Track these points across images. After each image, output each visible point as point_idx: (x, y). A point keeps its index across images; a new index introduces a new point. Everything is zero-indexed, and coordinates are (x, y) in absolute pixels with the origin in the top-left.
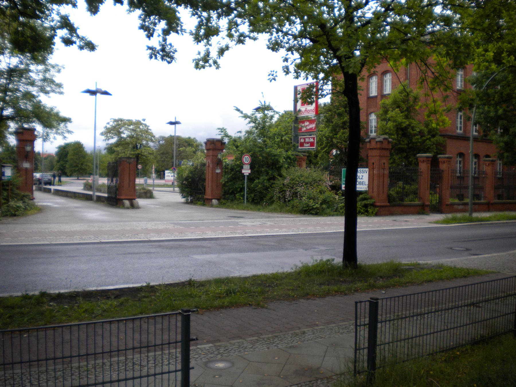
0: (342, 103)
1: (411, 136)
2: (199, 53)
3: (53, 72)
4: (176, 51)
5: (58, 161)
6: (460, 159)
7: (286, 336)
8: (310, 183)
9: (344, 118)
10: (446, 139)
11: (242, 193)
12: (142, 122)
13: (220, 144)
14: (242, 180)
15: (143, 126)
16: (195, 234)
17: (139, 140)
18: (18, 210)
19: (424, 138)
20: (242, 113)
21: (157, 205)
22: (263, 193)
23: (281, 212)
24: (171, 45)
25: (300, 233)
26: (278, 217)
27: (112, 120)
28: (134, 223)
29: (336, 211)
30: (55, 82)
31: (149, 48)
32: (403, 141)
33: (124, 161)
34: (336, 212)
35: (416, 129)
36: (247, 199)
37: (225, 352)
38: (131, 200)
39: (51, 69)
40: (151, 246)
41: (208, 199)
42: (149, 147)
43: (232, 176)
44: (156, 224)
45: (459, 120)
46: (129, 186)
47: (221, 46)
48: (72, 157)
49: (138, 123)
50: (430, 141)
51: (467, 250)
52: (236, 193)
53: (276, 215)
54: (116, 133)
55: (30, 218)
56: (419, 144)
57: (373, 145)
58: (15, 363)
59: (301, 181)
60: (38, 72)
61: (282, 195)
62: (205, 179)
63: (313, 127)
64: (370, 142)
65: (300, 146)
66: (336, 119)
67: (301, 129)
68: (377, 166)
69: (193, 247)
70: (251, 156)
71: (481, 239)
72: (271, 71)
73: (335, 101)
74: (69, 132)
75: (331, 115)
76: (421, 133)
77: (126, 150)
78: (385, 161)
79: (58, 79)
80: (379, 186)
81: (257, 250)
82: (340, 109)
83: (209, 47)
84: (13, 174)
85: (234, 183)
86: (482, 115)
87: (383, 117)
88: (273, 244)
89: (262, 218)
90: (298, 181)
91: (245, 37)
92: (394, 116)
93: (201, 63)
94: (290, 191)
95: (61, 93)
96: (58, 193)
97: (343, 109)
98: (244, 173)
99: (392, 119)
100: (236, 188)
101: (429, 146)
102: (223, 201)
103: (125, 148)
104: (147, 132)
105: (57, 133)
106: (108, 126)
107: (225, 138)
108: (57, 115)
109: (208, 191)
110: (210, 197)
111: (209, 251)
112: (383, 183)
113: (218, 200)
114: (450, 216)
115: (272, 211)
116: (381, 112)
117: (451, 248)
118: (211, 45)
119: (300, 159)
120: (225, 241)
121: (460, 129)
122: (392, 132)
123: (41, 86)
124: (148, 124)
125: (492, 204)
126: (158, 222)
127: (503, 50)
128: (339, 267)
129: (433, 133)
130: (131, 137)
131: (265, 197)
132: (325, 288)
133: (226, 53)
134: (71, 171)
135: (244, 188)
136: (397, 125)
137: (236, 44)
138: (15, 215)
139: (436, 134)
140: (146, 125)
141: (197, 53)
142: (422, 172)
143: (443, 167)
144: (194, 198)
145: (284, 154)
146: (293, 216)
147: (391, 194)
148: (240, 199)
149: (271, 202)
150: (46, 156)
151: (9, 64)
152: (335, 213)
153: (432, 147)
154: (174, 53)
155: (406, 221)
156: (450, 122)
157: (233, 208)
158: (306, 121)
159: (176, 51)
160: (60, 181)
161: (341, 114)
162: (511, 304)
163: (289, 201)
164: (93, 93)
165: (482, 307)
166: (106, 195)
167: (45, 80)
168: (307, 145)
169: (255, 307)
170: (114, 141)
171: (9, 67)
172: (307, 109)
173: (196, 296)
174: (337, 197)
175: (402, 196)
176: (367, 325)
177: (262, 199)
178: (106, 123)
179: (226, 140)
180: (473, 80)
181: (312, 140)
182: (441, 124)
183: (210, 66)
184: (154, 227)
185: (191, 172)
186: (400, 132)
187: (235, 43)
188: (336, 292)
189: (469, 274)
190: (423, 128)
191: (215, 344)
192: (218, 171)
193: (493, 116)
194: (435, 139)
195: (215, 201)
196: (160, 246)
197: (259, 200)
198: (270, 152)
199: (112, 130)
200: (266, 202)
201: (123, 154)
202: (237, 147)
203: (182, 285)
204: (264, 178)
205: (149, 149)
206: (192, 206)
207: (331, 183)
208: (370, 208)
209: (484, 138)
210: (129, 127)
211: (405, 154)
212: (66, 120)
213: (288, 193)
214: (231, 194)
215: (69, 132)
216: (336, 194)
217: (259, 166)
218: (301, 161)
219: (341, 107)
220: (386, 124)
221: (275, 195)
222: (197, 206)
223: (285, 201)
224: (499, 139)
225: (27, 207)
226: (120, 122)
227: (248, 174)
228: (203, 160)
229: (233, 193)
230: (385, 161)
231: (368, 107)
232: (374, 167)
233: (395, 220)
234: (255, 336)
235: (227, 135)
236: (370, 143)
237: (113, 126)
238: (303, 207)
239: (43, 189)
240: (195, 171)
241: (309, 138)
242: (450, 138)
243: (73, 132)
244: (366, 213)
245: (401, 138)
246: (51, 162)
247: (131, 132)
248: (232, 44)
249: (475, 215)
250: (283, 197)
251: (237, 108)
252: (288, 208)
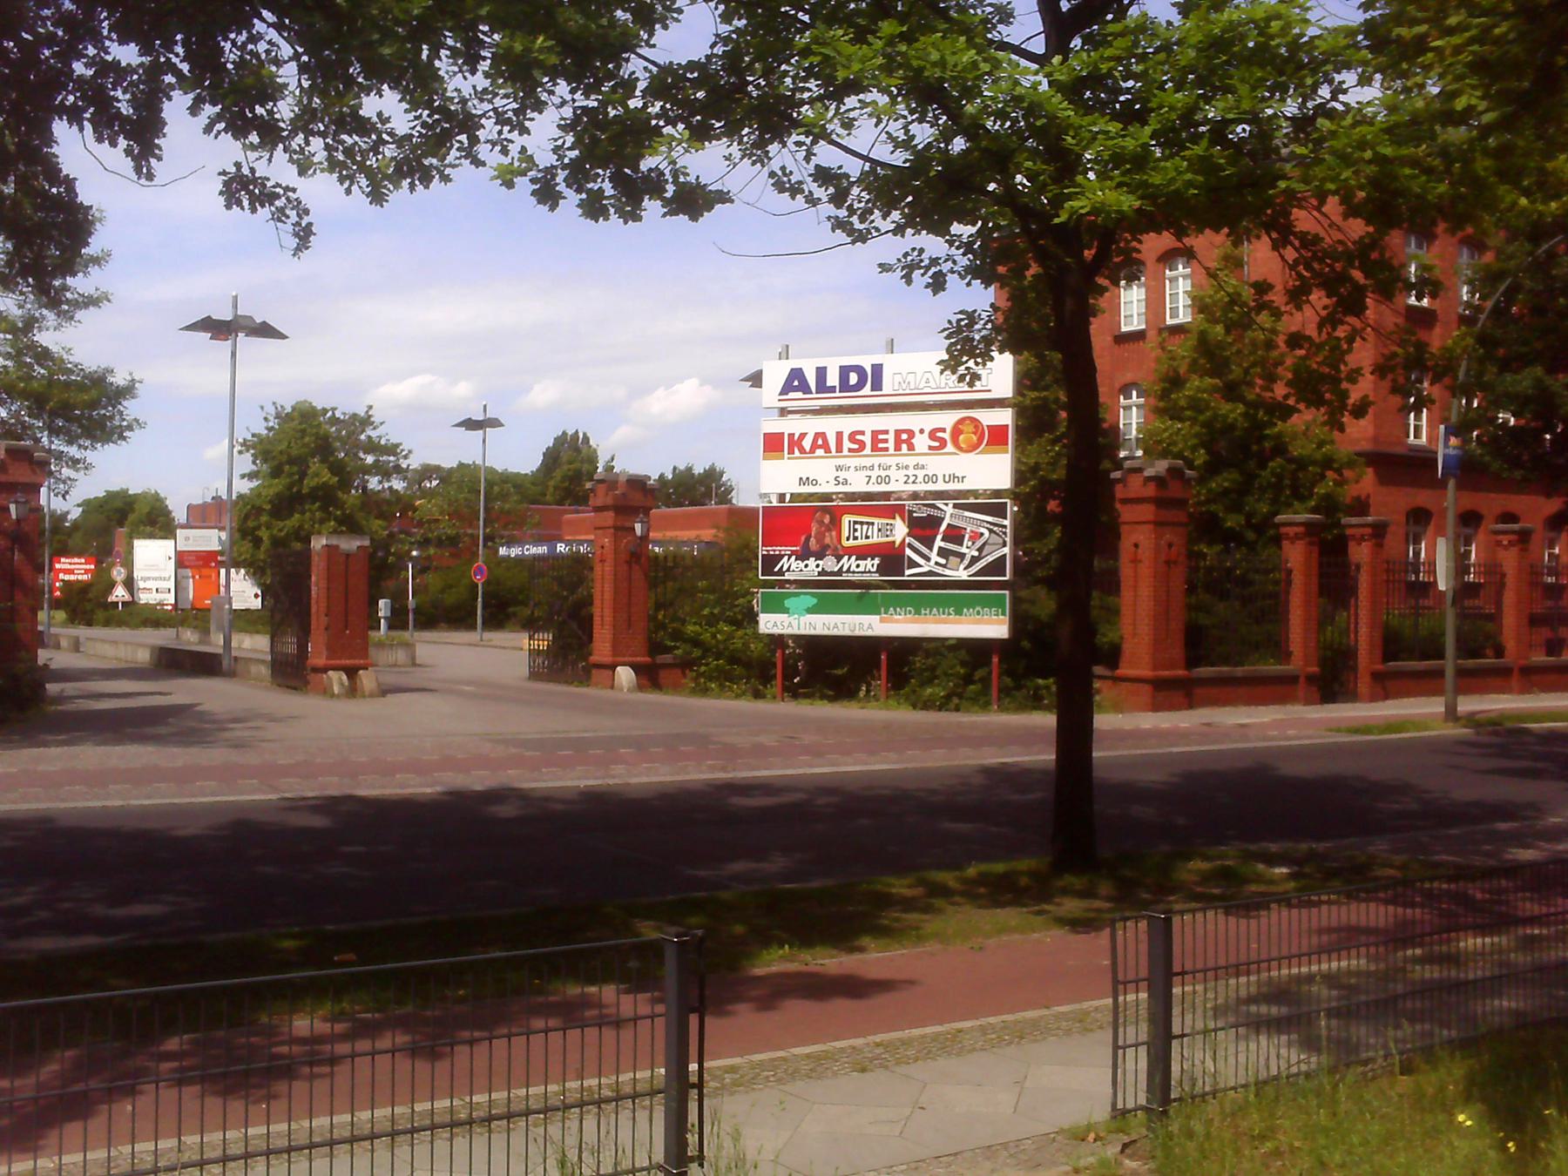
58: (359, 1055)
110: (608, 660)
143: (1360, 553)
166: (994, 627)
176: (1143, 1044)
227: (63, 560)
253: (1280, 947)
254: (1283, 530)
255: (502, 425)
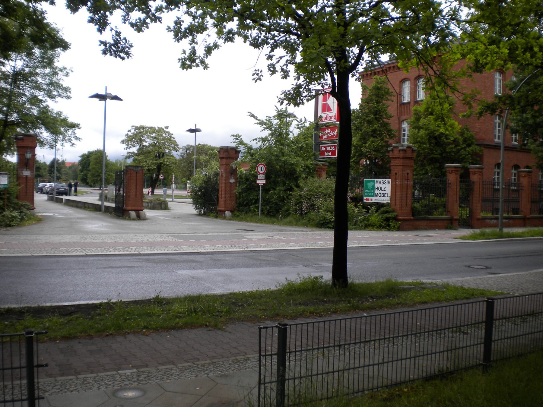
0: (372, 110)
1: (444, 146)
2: (184, 52)
3: (60, 75)
4: (132, 46)
5: (81, 171)
6: (515, 172)
7: (225, 363)
8: (329, 195)
9: (373, 126)
10: (482, 148)
11: (257, 205)
12: (165, 129)
13: (234, 152)
14: (257, 191)
15: (165, 134)
16: (192, 247)
17: (161, 148)
18: (13, 220)
19: (459, 148)
20: (256, 118)
21: (166, 216)
22: (279, 204)
23: (296, 225)
24: (125, 39)
25: (308, 248)
26: (291, 231)
27: (134, 128)
28: (132, 235)
29: (355, 224)
30: (62, 86)
31: (102, 42)
32: (436, 151)
33: (131, 170)
34: (322, 225)
35: (450, 137)
36: (262, 211)
37: (145, 379)
38: (137, 211)
39: (59, 72)
40: (138, 260)
41: (221, 211)
42: (172, 156)
43: (247, 186)
44: (154, 237)
45: (497, 128)
46: (136, 197)
47: (208, 43)
48: (94, 166)
49: (161, 131)
50: (465, 150)
51: (487, 268)
52: (251, 205)
53: (290, 228)
54: (137, 141)
55: (24, 229)
56: (453, 154)
57: (396, 154)
59: (319, 192)
60: (44, 75)
61: (298, 207)
62: (218, 190)
63: (334, 135)
64: (392, 150)
65: (321, 155)
66: (365, 127)
67: (322, 137)
68: (400, 177)
69: (184, 261)
70: (266, 165)
71: (506, 256)
72: (256, 70)
73: (364, 108)
74: (77, 138)
75: (361, 123)
76: (455, 141)
77: (148, 159)
78: (408, 171)
79: (65, 82)
80: (401, 198)
81: (253, 266)
82: (369, 117)
83: (195, 45)
84: (10, 182)
85: (249, 194)
86: (520, 123)
87: (415, 125)
88: (272, 259)
89: (272, 231)
90: (316, 193)
91: (233, 35)
92: (426, 123)
93: (188, 62)
94: (307, 203)
95: (68, 97)
96: (69, 203)
97: (373, 116)
98: (258, 184)
99: (424, 127)
100: (251, 200)
101: (464, 156)
102: (237, 213)
103: (147, 157)
104: (170, 140)
105: (64, 140)
106: (130, 134)
107: (240, 146)
108: (64, 120)
109: (222, 201)
111: (200, 265)
112: (407, 194)
113: (232, 212)
114: (478, 231)
115: (286, 224)
116: (413, 119)
117: (469, 266)
118: (196, 43)
119: (319, 168)
120: (222, 255)
121: (499, 138)
122: (424, 140)
123: (48, 91)
124: (171, 132)
125: (529, 219)
126: (157, 235)
127: (517, 47)
128: (326, 285)
129: (468, 142)
130: (154, 145)
131: (281, 209)
132: (301, 308)
133: (214, 52)
134: (93, 181)
135: (258, 199)
136: (429, 133)
137: (225, 42)
138: (10, 226)
139: (472, 143)
140: (169, 133)
141: (182, 51)
142: (450, 183)
143: (474, 178)
144: (207, 210)
145: (302, 163)
146: (309, 230)
147: (415, 207)
148: (255, 211)
149: (287, 214)
150: (70, 165)
151: (14, 67)
152: (354, 227)
153: (467, 157)
154: (129, 49)
155: (430, 236)
156: (460, 126)
157: (246, 221)
158: (327, 128)
159: (132, 46)
160: (76, 191)
161: (371, 122)
162: (505, 331)
163: (306, 213)
164: (102, 98)
165: (467, 334)
166: (113, 205)
167: (51, 84)
168: (328, 154)
169: (211, 329)
170: (135, 150)
171: (14, 71)
172: (328, 115)
173: (154, 314)
174: (356, 210)
175: (430, 209)
177: (278, 212)
178: (128, 130)
179: (242, 149)
180: (510, 84)
181: (333, 149)
182: (450, 129)
183: (198, 66)
184: (150, 240)
185: (205, 182)
186: (434, 141)
187: (223, 41)
188: (311, 313)
189: (473, 295)
190: (457, 136)
191: (138, 369)
192: (232, 181)
193: (532, 123)
194: (471, 148)
195: (228, 213)
196: (147, 260)
197: (275, 212)
198: (286, 160)
199: (133, 138)
200: (282, 215)
201: (145, 163)
202: (252, 155)
203: (148, 302)
204: (280, 188)
205: (171, 158)
206: (205, 218)
207: (352, 195)
208: (392, 222)
209: (523, 147)
210: (151, 135)
211: (438, 165)
212: (74, 126)
213: (305, 205)
214: (245, 206)
215: (77, 138)
216: (356, 206)
217: (276, 176)
218: (321, 171)
219: (371, 114)
220: (418, 132)
221: (292, 207)
222: (209, 219)
223: (302, 214)
224: (537, 148)
225: (25, 217)
226: (142, 130)
227: (263, 184)
228: (217, 170)
229: (247, 205)
230: (408, 171)
231: (400, 114)
232: (397, 178)
233: (417, 235)
234: (190, 362)
235: (241, 143)
236: (393, 152)
237: (135, 134)
238: (320, 220)
239: (55, 199)
240: (208, 181)
241: (330, 146)
242: (488, 148)
243: (81, 139)
244: (388, 227)
245: (434, 147)
246: (75, 171)
247: (153, 140)
248: (220, 42)
249: (506, 230)
250: (300, 209)
251: (251, 113)
252: (304, 221)
253: (507, 301)
254: (447, 169)
255: (201, 131)
